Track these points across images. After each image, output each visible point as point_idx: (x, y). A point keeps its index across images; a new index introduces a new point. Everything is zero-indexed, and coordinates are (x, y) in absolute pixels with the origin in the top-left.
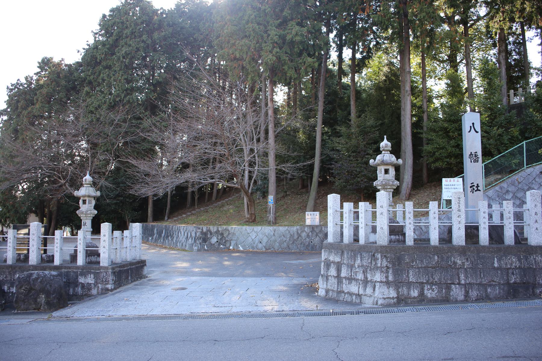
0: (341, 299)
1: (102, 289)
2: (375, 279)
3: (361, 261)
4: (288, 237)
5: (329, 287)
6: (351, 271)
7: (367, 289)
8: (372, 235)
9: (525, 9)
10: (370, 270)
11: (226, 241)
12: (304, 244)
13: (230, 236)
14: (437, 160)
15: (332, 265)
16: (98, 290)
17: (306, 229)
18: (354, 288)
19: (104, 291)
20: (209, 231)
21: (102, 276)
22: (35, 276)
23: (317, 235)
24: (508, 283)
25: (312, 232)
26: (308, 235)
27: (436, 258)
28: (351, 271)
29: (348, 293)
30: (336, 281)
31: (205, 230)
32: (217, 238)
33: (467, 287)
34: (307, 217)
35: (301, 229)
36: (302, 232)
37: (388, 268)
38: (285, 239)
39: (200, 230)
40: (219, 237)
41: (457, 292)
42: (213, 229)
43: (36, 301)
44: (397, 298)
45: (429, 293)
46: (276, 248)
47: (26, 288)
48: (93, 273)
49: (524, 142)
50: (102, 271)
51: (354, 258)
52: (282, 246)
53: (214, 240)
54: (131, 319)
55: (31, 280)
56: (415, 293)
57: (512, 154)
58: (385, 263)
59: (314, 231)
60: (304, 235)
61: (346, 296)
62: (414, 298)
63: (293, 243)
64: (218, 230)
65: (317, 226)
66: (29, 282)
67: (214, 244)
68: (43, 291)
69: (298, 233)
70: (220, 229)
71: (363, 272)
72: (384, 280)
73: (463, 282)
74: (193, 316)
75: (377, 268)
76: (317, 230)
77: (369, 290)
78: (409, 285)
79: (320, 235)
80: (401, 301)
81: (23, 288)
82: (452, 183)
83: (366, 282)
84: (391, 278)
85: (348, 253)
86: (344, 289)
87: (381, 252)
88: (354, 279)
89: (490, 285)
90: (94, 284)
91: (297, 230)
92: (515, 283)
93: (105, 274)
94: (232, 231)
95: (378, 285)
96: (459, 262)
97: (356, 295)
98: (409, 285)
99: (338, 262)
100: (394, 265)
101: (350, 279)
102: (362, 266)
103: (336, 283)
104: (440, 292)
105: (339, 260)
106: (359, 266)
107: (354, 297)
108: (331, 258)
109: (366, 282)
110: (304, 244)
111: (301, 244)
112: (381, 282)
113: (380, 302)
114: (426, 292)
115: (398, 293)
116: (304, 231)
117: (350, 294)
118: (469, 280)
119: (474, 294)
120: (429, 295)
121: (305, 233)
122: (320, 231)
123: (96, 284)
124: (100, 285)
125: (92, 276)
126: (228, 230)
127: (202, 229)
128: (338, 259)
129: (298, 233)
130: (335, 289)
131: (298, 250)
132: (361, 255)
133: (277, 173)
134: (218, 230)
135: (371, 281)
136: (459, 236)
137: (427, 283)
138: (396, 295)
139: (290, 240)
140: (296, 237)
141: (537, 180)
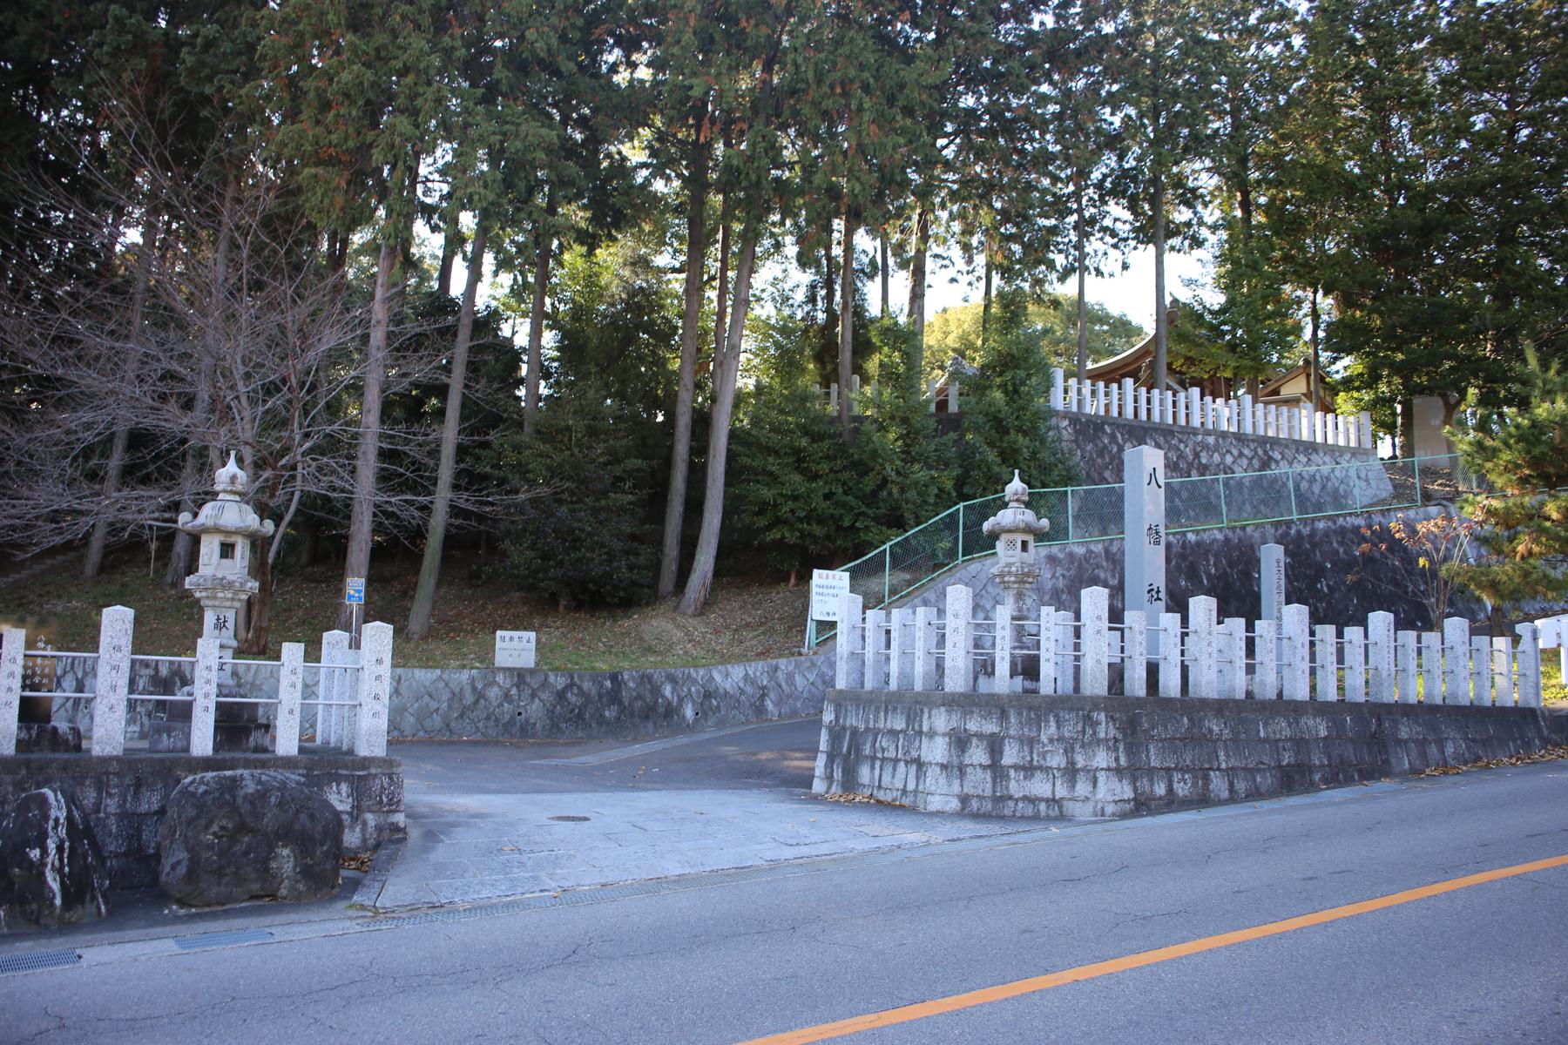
0: (1007, 812)
1: (379, 829)
2: (1095, 764)
3: (1058, 728)
4: (445, 698)
5: (968, 790)
6: (1031, 753)
7: (1078, 787)
8: (982, 680)
10: (1083, 747)
12: (497, 720)
14: (778, 522)
15: (974, 741)
16: (364, 830)
17: (500, 678)
18: (1040, 787)
19: (386, 835)
21: (376, 787)
22: (250, 787)
23: (533, 695)
24: (1280, 767)
25: (518, 686)
26: (507, 696)
27: (1186, 720)
28: (1031, 753)
29: (1025, 798)
30: (988, 776)
31: (164, 671)
33: (1231, 772)
34: (499, 644)
35: (484, 677)
37: (1116, 740)
38: (434, 705)
39: (150, 672)
41: (1219, 785)
43: (267, 869)
44: (1135, 799)
45: (1182, 789)
46: (408, 731)
47: (222, 828)
48: (346, 778)
49: (961, 505)
50: (373, 771)
51: (1038, 723)
52: (428, 723)
55: (239, 801)
56: (1160, 789)
57: (937, 530)
58: (1112, 732)
59: (525, 683)
60: (493, 693)
61: (1020, 805)
62: (1161, 798)
63: (462, 715)
65: (532, 672)
66: (234, 808)
68: (285, 834)
69: (474, 689)
71: (1066, 751)
72: (1114, 765)
73: (1223, 766)
74: (743, 871)
75: (1099, 742)
76: (535, 682)
77: (1082, 788)
78: (1151, 772)
79: (545, 696)
80: (1141, 806)
81: (215, 828)
82: (830, 582)
83: (1071, 773)
84: (1123, 761)
85: (1020, 714)
86: (1012, 792)
87: (1106, 710)
88: (1040, 768)
89: (1259, 770)
90: (350, 814)
91: (473, 680)
92: (1288, 765)
93: (386, 781)
94: (250, 678)
95: (1102, 777)
96: (1216, 728)
97: (1047, 801)
98: (1151, 772)
99: (992, 735)
100: (1125, 736)
101: (1029, 770)
102: (1061, 739)
103: (989, 779)
104: (1194, 785)
105: (996, 729)
106: (1051, 741)
107: (1043, 806)
108: (973, 726)
109: (1071, 773)
110: (497, 720)
111: (488, 718)
112: (1109, 769)
113: (1110, 809)
114: (1175, 785)
115: (1135, 790)
116: (494, 682)
117: (1032, 800)
118: (1233, 763)
119: (1241, 786)
120: (1180, 793)
121: (496, 689)
123: (357, 812)
124: (369, 817)
125: (344, 787)
127: (156, 669)
128: (990, 727)
129: (474, 689)
130: (988, 793)
131: (479, 737)
132: (1056, 716)
133: (375, 515)
135: (1085, 769)
136: (1136, 683)
137: (1176, 769)
138: (1132, 795)
139: (450, 706)
140: (469, 699)
141: (990, 589)
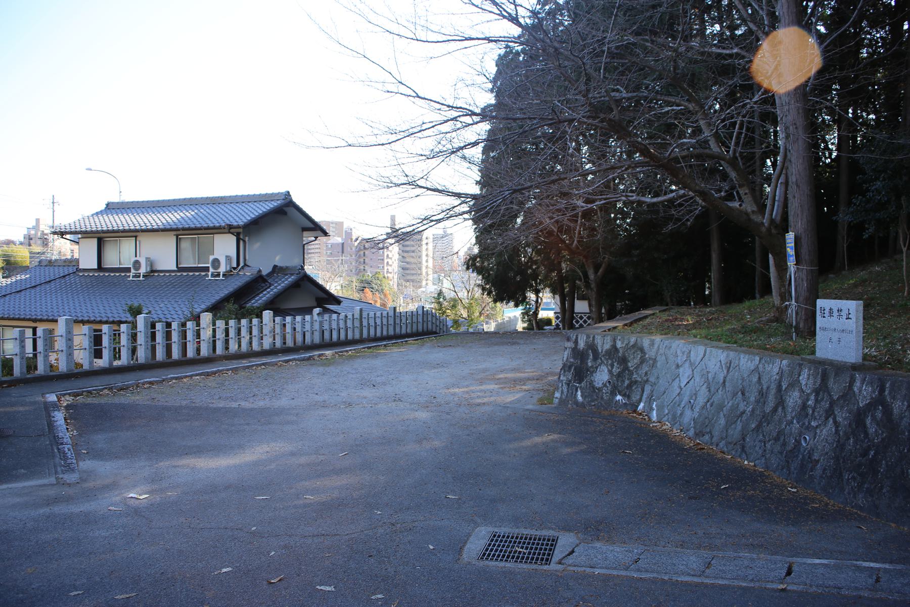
9: (737, 53)
11: (633, 383)
13: (645, 368)
20: (592, 347)
23: (829, 413)
31: (582, 345)
32: (610, 372)
36: (791, 385)
40: (616, 370)
42: (604, 344)
53: (602, 376)
54: (408, 335)
64: (614, 346)
67: (600, 389)
70: (619, 344)
122: (843, 397)
126: (642, 350)
127: (576, 342)
134: (614, 346)
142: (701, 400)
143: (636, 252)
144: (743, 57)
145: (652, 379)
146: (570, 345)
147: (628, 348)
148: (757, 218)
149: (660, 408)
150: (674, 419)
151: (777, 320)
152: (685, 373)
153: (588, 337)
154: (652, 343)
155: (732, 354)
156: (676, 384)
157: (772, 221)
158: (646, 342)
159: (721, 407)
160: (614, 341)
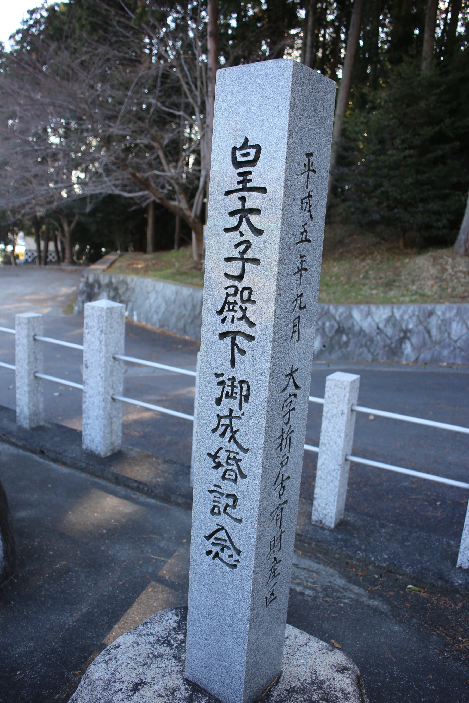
13: (128, 293)
20: (97, 281)
42: (104, 280)
70: (114, 280)
126: (126, 283)
127: (87, 278)
142: (162, 309)
143: (100, 215)
144: (341, 593)
145: (133, 299)
146: (83, 280)
147: (119, 282)
148: (187, 213)
149: (138, 315)
150: (147, 320)
151: (195, 268)
152: (153, 296)
153: (95, 275)
154: (132, 280)
155: (179, 287)
156: (147, 302)
157: (196, 215)
158: (129, 279)
159: (173, 313)
160: (111, 278)
